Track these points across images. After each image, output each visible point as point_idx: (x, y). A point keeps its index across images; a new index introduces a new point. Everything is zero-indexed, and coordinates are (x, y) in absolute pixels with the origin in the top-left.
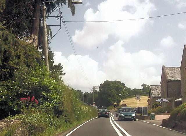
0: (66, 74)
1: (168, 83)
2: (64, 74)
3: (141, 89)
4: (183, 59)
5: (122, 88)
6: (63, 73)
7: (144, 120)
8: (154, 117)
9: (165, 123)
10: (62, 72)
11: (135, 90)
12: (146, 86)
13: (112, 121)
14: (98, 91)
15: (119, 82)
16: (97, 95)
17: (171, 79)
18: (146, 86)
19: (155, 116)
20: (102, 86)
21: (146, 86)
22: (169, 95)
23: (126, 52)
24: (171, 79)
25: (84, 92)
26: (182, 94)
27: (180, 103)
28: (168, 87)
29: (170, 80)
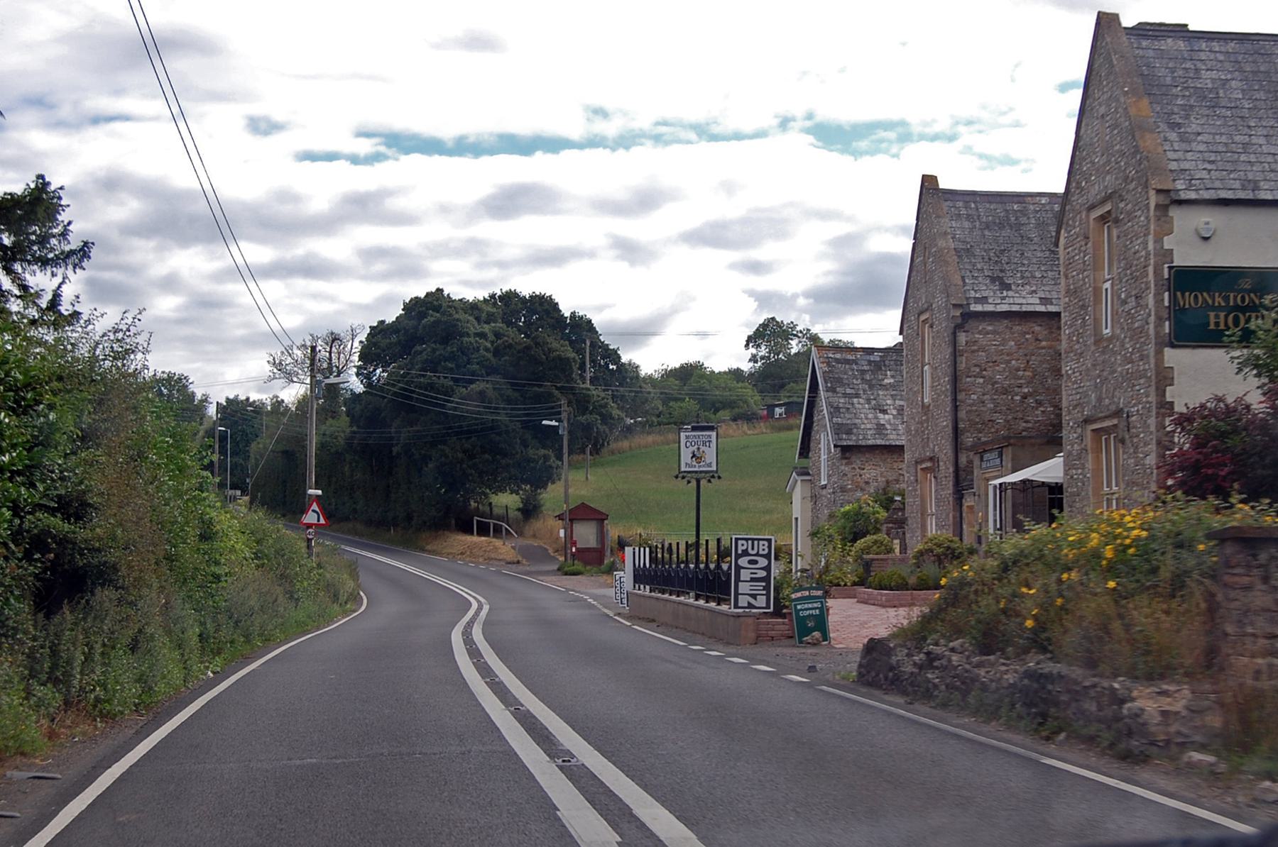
0: (94, 252)
1: (962, 338)
2: (83, 253)
3: (746, 367)
4: (1085, 139)
5: (562, 366)
6: (74, 244)
7: (732, 649)
8: (821, 623)
9: (877, 667)
10: (64, 235)
11: (689, 374)
12: (794, 343)
13: (474, 653)
14: (355, 384)
15: (543, 306)
16: (341, 426)
17: (984, 300)
18: (795, 347)
19: (824, 611)
20: (383, 343)
21: (795, 347)
22: (968, 440)
23: (440, 291)
24: (984, 300)
25: (219, 395)
26: (1068, 435)
27: (1049, 500)
28: (962, 366)
29: (979, 308)
